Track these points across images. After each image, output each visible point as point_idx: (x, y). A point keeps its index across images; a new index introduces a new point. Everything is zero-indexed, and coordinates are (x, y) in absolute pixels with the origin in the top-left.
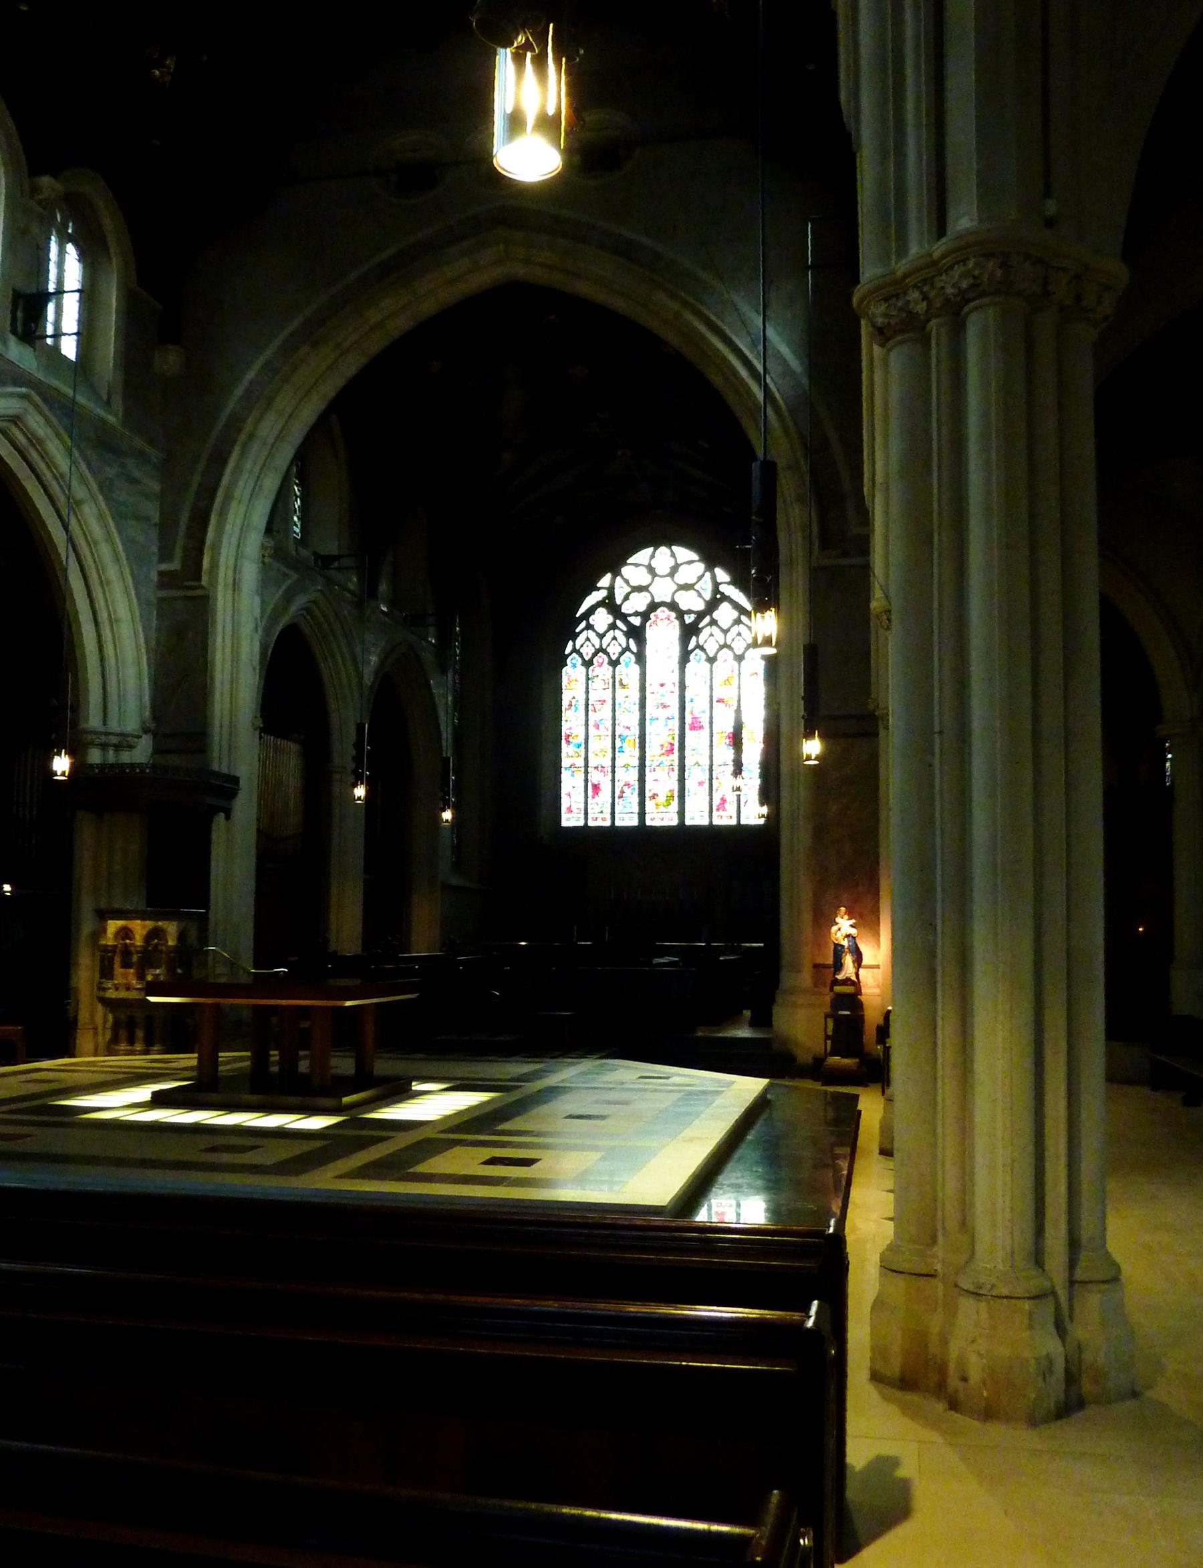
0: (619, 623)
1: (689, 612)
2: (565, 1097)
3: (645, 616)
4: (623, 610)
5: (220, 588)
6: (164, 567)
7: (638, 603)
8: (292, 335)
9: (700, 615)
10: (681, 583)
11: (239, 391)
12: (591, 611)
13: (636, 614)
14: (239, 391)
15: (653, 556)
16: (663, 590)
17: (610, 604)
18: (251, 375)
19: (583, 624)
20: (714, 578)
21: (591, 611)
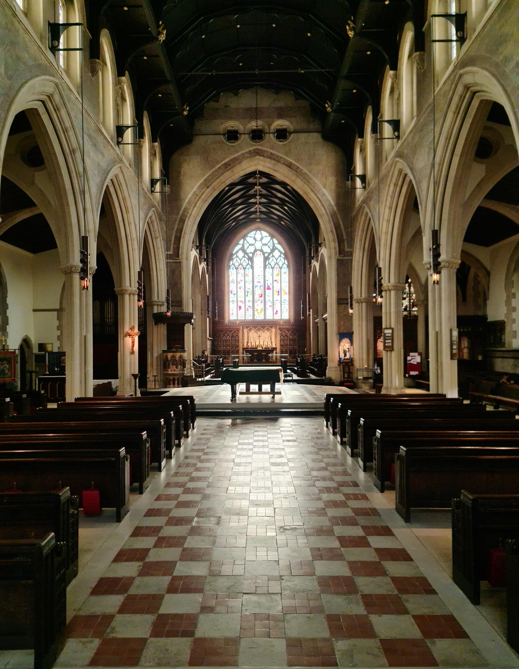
0: (246, 256)
1: (266, 253)
3: (253, 254)
7: (251, 250)
9: (269, 254)
10: (264, 243)
11: (187, 201)
12: (237, 252)
13: (251, 253)
14: (187, 201)
15: (255, 234)
16: (258, 245)
17: (243, 249)
18: (190, 196)
19: (235, 256)
20: (273, 241)
21: (237, 252)
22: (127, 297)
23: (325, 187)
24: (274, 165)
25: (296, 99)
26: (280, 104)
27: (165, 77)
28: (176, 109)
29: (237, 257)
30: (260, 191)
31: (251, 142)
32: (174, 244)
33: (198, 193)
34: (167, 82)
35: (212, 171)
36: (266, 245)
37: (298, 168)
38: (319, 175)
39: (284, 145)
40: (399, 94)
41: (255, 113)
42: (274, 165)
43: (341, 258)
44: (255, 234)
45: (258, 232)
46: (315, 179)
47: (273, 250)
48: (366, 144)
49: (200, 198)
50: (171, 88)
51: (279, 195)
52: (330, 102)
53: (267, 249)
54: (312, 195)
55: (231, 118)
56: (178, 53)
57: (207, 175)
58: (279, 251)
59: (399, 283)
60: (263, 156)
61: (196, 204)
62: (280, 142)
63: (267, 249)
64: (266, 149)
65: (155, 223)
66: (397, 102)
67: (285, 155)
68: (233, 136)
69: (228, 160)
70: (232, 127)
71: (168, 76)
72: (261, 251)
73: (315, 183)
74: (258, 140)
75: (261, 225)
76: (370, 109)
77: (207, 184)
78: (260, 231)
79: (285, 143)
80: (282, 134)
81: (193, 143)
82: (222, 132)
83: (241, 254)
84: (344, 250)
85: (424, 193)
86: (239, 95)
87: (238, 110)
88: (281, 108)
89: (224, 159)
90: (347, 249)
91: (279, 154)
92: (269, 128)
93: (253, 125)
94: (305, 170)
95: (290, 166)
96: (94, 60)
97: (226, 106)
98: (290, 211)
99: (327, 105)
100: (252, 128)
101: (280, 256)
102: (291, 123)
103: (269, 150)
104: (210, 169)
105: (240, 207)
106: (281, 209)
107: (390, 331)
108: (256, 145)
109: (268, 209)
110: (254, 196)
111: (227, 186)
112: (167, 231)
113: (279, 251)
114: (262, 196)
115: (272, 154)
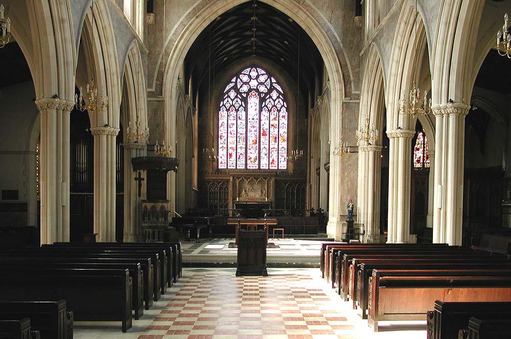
0: (239, 96)
1: (263, 93)
6: (148, 90)
7: (245, 88)
9: (266, 94)
11: (173, 32)
12: (229, 91)
13: (245, 92)
14: (173, 32)
15: (250, 71)
16: (254, 83)
17: (235, 88)
18: (176, 26)
19: (226, 96)
21: (229, 91)
23: (330, 22)
43: (347, 101)
44: (250, 71)
51: (279, 28)
53: (262, 89)
57: (196, 4)
58: (278, 91)
72: (257, 90)
75: (257, 61)
77: (195, 13)
83: (232, 94)
84: (350, 92)
90: (353, 92)
105: (233, 40)
111: (219, 16)
113: (278, 91)
114: (259, 28)
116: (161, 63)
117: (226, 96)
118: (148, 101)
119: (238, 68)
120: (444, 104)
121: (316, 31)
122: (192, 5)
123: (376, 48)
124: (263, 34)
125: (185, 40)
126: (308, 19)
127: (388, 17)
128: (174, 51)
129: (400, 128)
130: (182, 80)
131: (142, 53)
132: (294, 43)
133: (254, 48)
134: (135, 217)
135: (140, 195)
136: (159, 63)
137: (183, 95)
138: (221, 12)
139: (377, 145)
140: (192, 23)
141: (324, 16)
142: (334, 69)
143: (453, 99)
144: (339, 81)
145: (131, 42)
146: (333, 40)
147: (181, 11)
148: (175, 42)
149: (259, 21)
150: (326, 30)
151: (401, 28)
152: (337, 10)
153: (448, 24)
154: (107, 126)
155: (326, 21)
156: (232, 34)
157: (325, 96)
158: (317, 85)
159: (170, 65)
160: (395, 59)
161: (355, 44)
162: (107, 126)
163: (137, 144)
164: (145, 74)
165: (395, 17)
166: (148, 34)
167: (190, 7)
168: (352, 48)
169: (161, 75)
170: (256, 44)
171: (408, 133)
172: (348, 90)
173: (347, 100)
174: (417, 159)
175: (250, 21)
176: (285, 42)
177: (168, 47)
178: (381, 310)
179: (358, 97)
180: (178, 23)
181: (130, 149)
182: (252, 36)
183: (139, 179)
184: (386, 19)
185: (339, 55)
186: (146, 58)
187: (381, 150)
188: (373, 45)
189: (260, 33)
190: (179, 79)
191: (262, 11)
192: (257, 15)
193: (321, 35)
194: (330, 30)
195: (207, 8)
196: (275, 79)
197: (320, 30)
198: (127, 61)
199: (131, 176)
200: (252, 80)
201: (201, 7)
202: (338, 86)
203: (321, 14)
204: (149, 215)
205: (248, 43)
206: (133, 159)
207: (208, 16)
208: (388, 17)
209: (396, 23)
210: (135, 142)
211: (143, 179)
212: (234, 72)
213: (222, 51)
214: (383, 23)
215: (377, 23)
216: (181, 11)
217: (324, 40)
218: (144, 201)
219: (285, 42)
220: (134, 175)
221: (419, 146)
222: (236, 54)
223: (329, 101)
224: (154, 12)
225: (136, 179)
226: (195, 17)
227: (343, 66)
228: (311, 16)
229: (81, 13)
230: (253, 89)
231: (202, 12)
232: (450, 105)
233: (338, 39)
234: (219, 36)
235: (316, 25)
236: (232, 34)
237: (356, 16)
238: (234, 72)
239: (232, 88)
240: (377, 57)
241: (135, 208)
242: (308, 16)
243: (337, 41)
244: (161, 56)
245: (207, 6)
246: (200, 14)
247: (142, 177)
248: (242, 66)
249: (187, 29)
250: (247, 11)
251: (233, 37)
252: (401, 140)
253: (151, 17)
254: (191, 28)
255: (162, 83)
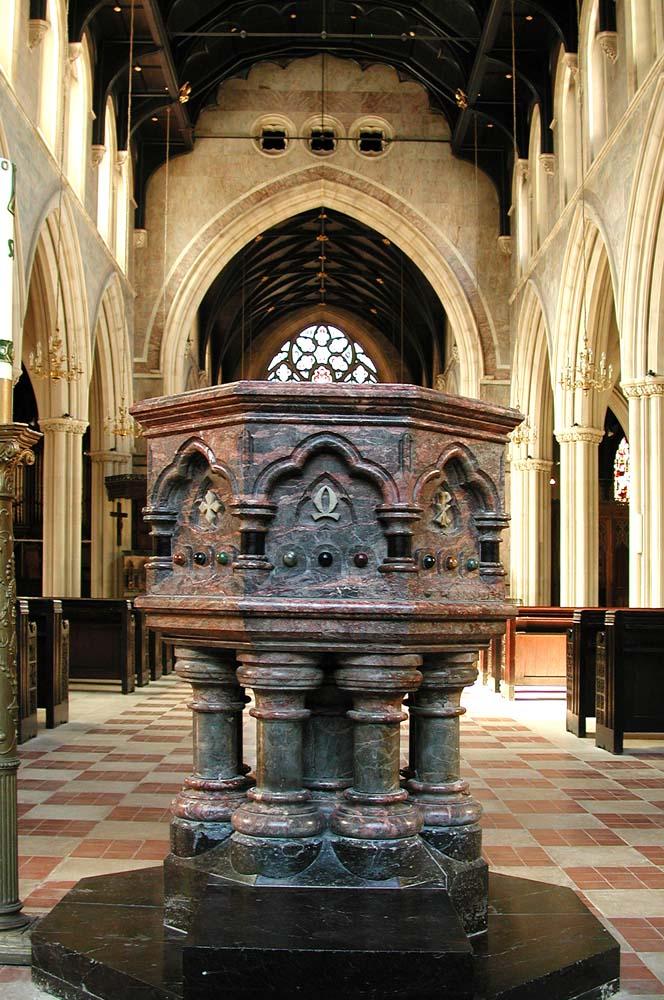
0: (295, 376)
1: (339, 370)
2: (133, 789)
3: (311, 372)
4: (298, 367)
5: (169, 373)
6: (136, 360)
7: (306, 363)
8: (208, 229)
9: (345, 373)
10: (325, 343)
11: (179, 260)
12: (278, 367)
13: (306, 370)
14: (179, 260)
15: (316, 332)
16: (322, 355)
17: (289, 362)
18: (185, 251)
19: (272, 375)
20: (353, 349)
21: (278, 367)
22: (62, 436)
23: (456, 246)
24: (357, 198)
25: (401, 81)
26: (370, 87)
27: (152, 40)
28: (167, 92)
29: (276, 377)
30: (327, 246)
31: (311, 154)
32: (150, 343)
33: (200, 246)
34: (154, 48)
35: (231, 206)
36: (338, 354)
37: (403, 205)
38: (446, 222)
39: (377, 162)
40: (582, 94)
41: (323, 101)
42: (357, 198)
43: (488, 382)
44: (316, 332)
45: (322, 328)
46: (435, 228)
47: (353, 367)
48: (533, 171)
49: (205, 256)
50: (162, 58)
51: (367, 256)
52: (465, 92)
53: (339, 364)
54: (431, 259)
55: (271, 109)
56: (189, 56)
57: (221, 213)
58: (367, 368)
59: (593, 427)
60: (334, 180)
61: (197, 266)
62: (370, 155)
63: (339, 364)
64: (337, 168)
65: (116, 301)
66: (580, 105)
67: (377, 181)
68: (273, 141)
69: (264, 185)
70: (274, 125)
71: (157, 39)
72: (328, 366)
73: (438, 235)
74: (323, 151)
75: (329, 315)
76: (536, 109)
77: (219, 229)
78: (326, 327)
79: (378, 158)
80: (371, 142)
81: (195, 152)
82: (252, 134)
83: (284, 372)
84: (494, 366)
85: (621, 263)
86: (288, 68)
87: (286, 98)
88: (371, 94)
89: (256, 183)
90: (499, 366)
91: (366, 179)
92: (347, 131)
93: (316, 122)
94: (417, 211)
95: (387, 201)
96: (35, 21)
97: (261, 87)
98: (388, 285)
99: (457, 96)
100: (314, 128)
101: (368, 379)
102: (390, 122)
103: (346, 170)
104: (228, 203)
105: (285, 277)
106: (370, 285)
107: (338, 377)
108: (319, 160)
109: (341, 282)
110: (314, 256)
111: (260, 235)
112: (135, 317)
113: (367, 368)
114: (331, 256)
115: (351, 177)
116: (157, 313)
117: (272, 375)
118: (134, 379)
119: (294, 327)
120: (641, 378)
121: (431, 259)
122: (213, 215)
123: (534, 290)
124: (339, 266)
125: (201, 274)
126: (418, 240)
127: (551, 236)
128: (182, 293)
129: (576, 425)
130: (194, 345)
131: (127, 296)
132: (395, 282)
133: (322, 291)
134: (112, 582)
135: (119, 544)
136: (154, 314)
137: (195, 369)
138: (263, 228)
139: (543, 459)
140: (213, 245)
141: (444, 235)
142: (464, 325)
143: (655, 371)
144: (474, 347)
145: (108, 276)
146: (462, 276)
147: (194, 225)
148: (182, 278)
149: (330, 244)
150: (449, 258)
151: (572, 254)
152: (467, 226)
153: (641, 248)
154: (67, 415)
155: (449, 243)
156: (283, 265)
157: (451, 372)
158: (436, 357)
159: (173, 316)
160: (565, 307)
161: (498, 278)
162: (67, 415)
163: (114, 452)
164: (130, 333)
165: (561, 237)
166: (137, 264)
167: (210, 219)
168: (494, 290)
169: (158, 334)
170: (329, 250)
171: (592, 434)
172: (489, 363)
173: (488, 380)
174: (619, 492)
175: (315, 244)
176: (378, 280)
177: (170, 288)
178: (519, 671)
179: (507, 375)
180: (189, 246)
181: (102, 462)
182: (318, 270)
183: (119, 515)
184: (548, 240)
185: (474, 303)
186: (132, 306)
187: (549, 469)
188: (530, 285)
189: (333, 265)
190: (188, 341)
191: (335, 226)
192: (327, 233)
193: (441, 267)
194: (457, 259)
195: (238, 221)
196: (361, 345)
197: (438, 259)
198: (101, 313)
199: (103, 507)
200: (319, 362)
201: (230, 219)
202: (471, 355)
203: (439, 232)
204: (136, 578)
205: (311, 282)
206: (107, 479)
207: (241, 234)
208: (551, 236)
209: (564, 246)
210: (112, 450)
211: (125, 515)
212: (287, 332)
213: (270, 291)
214: (544, 247)
215: (535, 248)
216: (194, 225)
217: (445, 277)
218: (127, 553)
219: (378, 280)
220: (110, 507)
221: (623, 467)
222: (288, 302)
223: (457, 383)
224: (147, 226)
225: (113, 514)
226: (218, 236)
227: (480, 322)
228: (422, 235)
229: (33, 228)
230: (322, 364)
231: (230, 228)
232: (650, 379)
233: (472, 276)
234: (259, 269)
235: (430, 249)
236: (283, 265)
237: (501, 235)
238: (287, 332)
239: (283, 362)
240: (532, 293)
241: (112, 565)
242: (417, 235)
243: (467, 278)
244: (158, 301)
245: (238, 219)
246: (227, 232)
247: (123, 511)
248: (301, 322)
249: (205, 256)
250: (310, 225)
251: (284, 271)
252: (580, 446)
253: (142, 234)
254: (210, 255)
255: (160, 347)
